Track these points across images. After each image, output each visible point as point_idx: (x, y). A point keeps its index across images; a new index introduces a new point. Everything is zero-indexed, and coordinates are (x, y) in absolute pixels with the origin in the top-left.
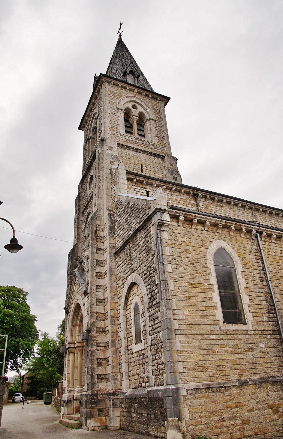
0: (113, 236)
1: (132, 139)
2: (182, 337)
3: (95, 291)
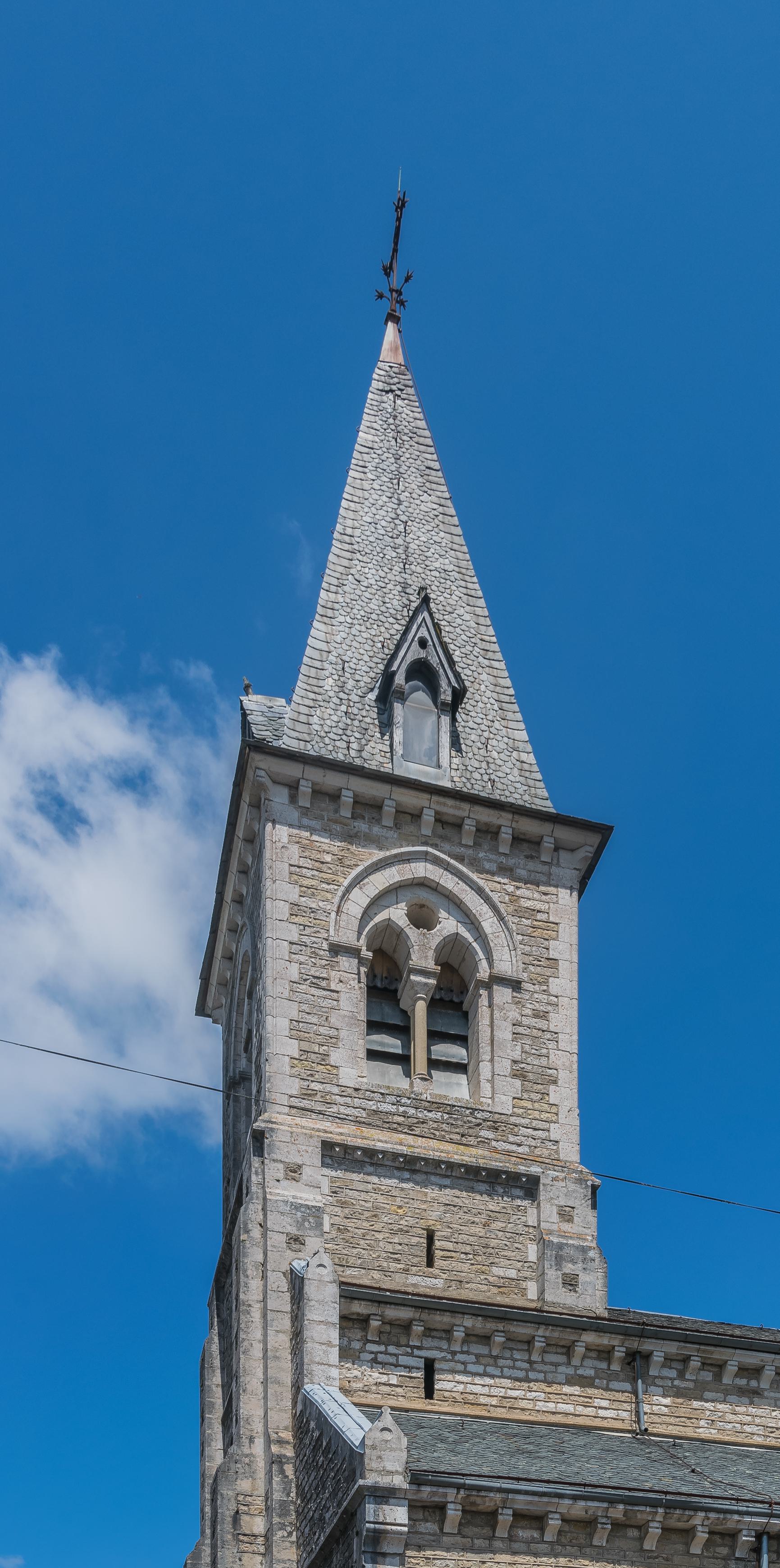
0: (288, 1536)
1: (393, 1109)
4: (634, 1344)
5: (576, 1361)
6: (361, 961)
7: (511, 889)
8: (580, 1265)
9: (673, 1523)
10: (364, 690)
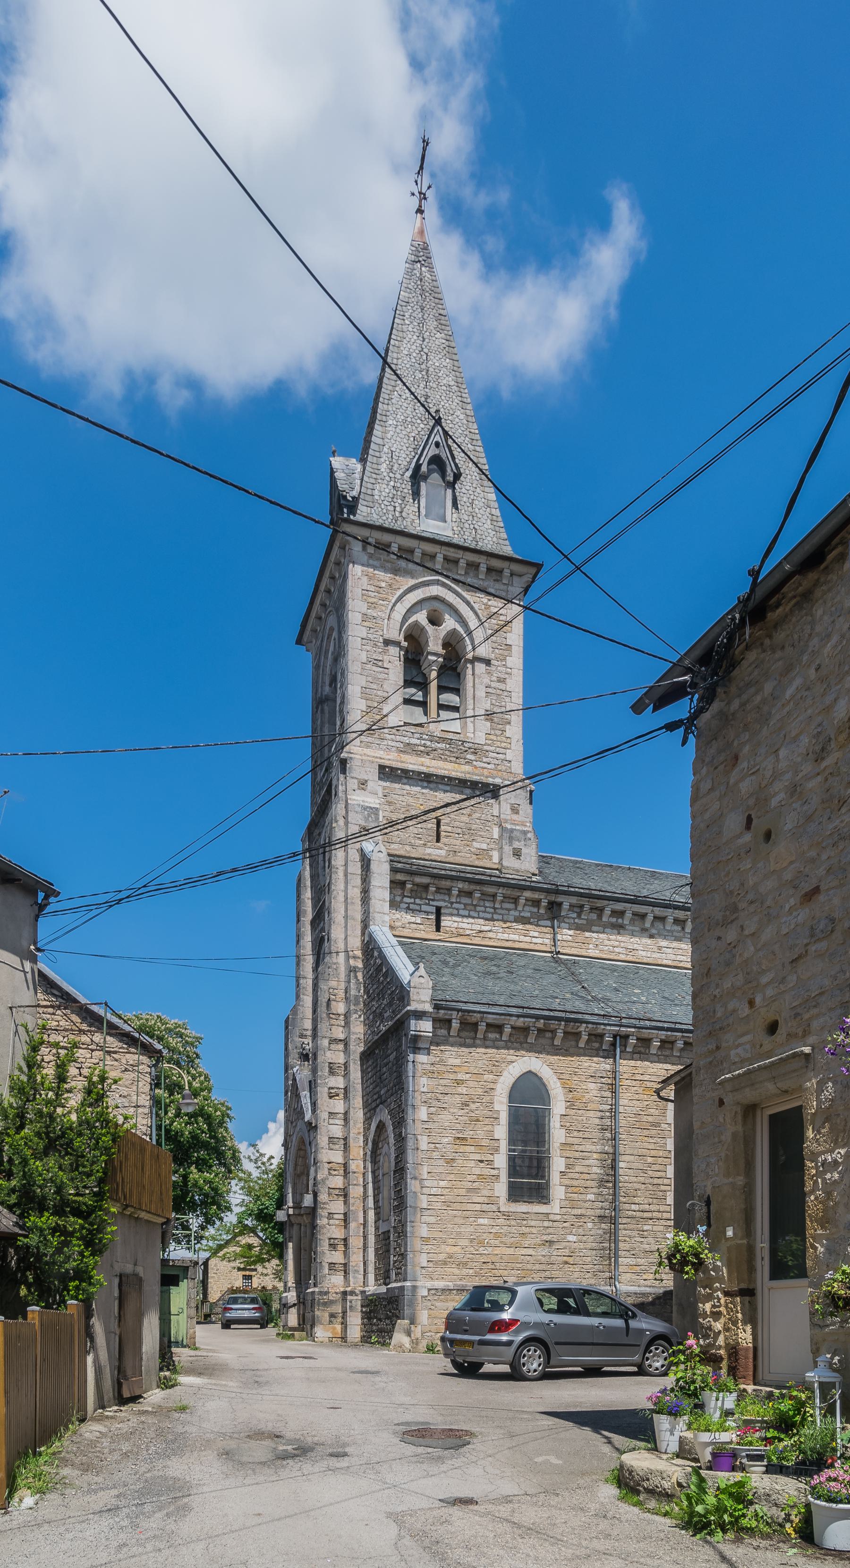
1: (418, 742)
2: (432, 1220)
3: (326, 1124)
4: (552, 898)
5: (520, 908)
6: (401, 648)
7: (485, 601)
8: (523, 842)
9: (569, 1030)
10: (404, 470)
